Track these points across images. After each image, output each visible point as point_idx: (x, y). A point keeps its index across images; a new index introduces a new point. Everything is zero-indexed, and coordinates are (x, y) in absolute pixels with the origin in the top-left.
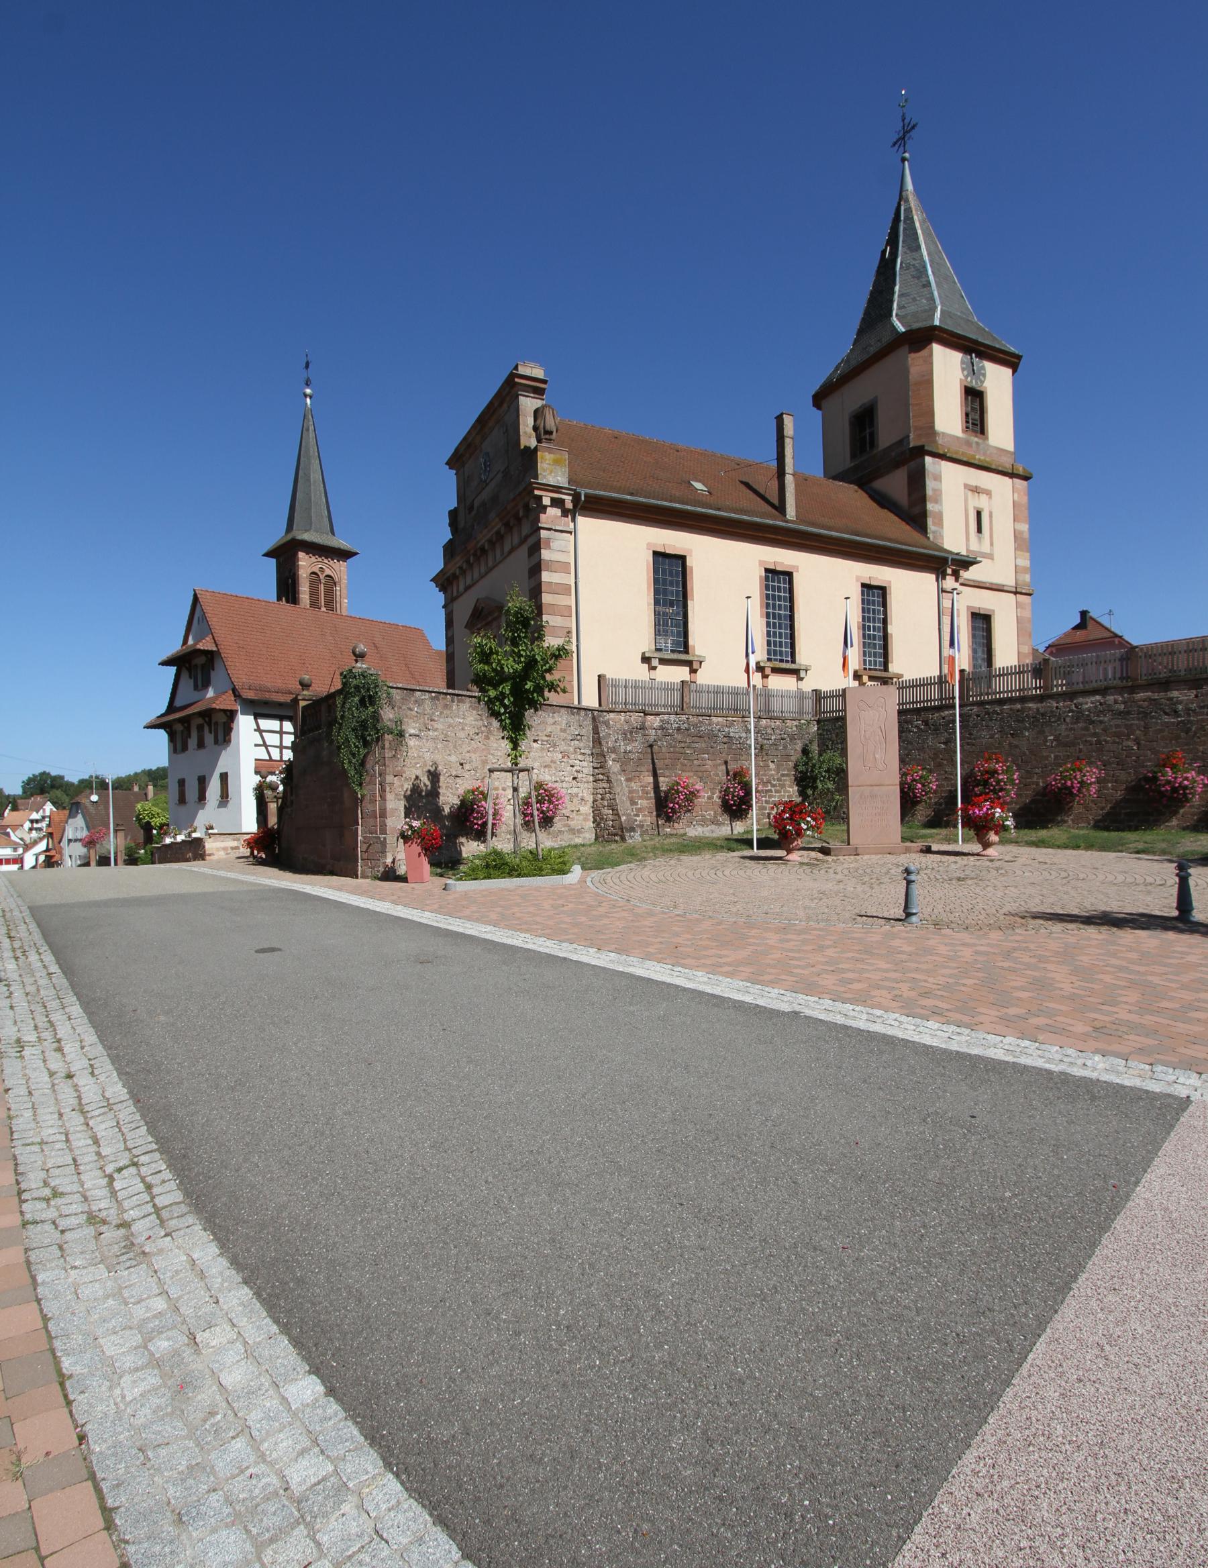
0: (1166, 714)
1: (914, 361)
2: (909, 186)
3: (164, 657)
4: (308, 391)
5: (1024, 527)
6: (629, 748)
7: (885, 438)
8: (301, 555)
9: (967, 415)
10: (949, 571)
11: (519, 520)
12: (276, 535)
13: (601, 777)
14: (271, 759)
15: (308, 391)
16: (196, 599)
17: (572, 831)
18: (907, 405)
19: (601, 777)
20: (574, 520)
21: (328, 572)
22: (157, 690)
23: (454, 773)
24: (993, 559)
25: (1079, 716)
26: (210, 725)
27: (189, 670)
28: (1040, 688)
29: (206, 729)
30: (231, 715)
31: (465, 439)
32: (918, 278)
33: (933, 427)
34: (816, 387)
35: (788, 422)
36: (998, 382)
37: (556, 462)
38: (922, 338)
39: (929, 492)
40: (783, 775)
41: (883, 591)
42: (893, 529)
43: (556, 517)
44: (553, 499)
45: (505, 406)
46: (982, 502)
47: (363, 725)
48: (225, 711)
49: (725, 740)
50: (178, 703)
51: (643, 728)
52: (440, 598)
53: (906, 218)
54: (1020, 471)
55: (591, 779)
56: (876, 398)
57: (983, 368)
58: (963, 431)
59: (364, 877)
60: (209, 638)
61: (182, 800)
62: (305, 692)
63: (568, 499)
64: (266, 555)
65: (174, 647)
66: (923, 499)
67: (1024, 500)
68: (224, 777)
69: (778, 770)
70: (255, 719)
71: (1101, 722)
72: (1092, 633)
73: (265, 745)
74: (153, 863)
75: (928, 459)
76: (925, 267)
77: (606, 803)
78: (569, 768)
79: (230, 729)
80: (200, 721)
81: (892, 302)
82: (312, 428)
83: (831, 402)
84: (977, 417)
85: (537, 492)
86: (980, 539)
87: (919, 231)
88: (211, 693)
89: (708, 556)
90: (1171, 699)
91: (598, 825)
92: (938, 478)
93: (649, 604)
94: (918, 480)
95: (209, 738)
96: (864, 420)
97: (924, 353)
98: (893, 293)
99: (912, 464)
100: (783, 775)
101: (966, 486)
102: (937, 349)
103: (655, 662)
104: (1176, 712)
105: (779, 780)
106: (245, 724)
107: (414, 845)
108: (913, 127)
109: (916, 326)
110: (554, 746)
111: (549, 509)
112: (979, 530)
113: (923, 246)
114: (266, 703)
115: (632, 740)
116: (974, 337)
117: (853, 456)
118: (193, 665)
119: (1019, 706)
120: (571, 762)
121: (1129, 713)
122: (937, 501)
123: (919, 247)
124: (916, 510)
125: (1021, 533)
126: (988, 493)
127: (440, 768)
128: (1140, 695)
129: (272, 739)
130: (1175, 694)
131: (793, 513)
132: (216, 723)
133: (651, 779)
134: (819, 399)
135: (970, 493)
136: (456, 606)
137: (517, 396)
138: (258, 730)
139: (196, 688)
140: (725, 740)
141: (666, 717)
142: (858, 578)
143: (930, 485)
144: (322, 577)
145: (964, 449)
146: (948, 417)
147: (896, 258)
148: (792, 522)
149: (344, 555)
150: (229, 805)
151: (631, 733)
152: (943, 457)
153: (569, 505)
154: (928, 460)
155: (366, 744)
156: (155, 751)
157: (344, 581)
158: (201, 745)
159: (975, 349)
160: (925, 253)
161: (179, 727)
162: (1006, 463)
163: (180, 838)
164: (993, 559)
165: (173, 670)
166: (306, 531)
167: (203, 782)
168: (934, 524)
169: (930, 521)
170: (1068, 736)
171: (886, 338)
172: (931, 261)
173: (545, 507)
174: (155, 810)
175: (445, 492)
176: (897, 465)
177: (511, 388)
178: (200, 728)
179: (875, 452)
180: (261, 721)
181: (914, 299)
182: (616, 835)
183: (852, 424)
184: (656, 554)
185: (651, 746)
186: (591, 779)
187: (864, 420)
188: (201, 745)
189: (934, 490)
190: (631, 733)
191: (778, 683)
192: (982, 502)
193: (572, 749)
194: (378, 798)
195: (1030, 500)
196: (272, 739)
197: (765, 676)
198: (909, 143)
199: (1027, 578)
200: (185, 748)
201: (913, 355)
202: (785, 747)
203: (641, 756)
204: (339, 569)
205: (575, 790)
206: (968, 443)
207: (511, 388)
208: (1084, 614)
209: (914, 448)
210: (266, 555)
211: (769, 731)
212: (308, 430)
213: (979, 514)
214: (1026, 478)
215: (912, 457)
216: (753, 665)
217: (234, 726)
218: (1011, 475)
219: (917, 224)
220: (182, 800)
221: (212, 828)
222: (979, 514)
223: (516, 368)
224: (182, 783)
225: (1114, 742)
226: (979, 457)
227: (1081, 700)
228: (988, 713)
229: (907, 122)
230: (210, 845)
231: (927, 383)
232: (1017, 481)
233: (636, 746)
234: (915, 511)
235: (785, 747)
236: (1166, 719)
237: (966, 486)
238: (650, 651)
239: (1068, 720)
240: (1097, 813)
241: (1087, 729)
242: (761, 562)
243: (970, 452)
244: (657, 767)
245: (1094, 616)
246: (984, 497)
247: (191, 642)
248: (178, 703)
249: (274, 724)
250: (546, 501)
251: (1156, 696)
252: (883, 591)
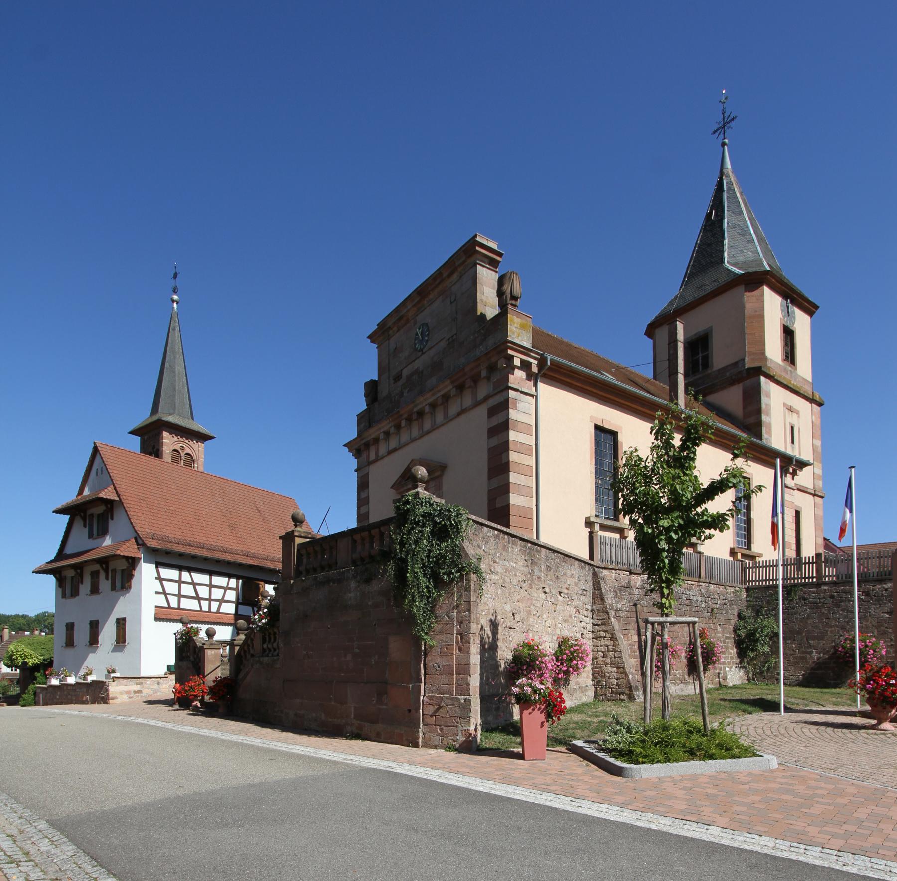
1: (749, 298)
3: (59, 505)
4: (176, 297)
5: (818, 443)
6: (619, 606)
7: (720, 359)
8: (165, 434)
11: (476, 379)
12: (142, 416)
13: (603, 634)
14: (169, 607)
15: (176, 297)
16: (96, 450)
18: (743, 334)
19: (603, 634)
20: (535, 385)
21: (188, 451)
22: (48, 536)
23: (509, 624)
26: (106, 571)
27: (84, 519)
28: (833, 576)
29: (102, 575)
30: (132, 563)
31: (397, 310)
33: (764, 353)
34: (651, 318)
36: (802, 323)
37: (523, 327)
38: (754, 280)
39: (763, 406)
43: (521, 379)
44: (522, 361)
45: (455, 277)
46: (793, 419)
47: (439, 561)
48: (127, 558)
49: (687, 602)
50: (68, 550)
51: (629, 586)
52: (353, 463)
53: (729, 189)
54: (817, 398)
55: (591, 635)
56: (711, 329)
57: (794, 312)
59: (427, 745)
60: (111, 488)
61: (70, 642)
62: (298, 529)
63: (534, 362)
64: (133, 432)
65: (70, 497)
66: (759, 411)
67: (818, 422)
68: (121, 623)
69: (723, 632)
70: (157, 567)
73: (164, 593)
74: (36, 704)
75: (763, 379)
77: (609, 661)
79: (131, 576)
80: (97, 567)
81: (722, 252)
82: (177, 329)
85: (510, 352)
87: (740, 200)
88: (108, 541)
91: (598, 683)
94: (753, 398)
95: (105, 584)
96: (699, 346)
97: (756, 293)
98: (723, 245)
99: (748, 382)
100: (726, 638)
105: (724, 642)
106: (147, 571)
107: (537, 713)
108: (733, 119)
109: (751, 270)
111: (516, 371)
112: (793, 442)
113: (744, 212)
114: (168, 553)
118: (90, 513)
122: (768, 414)
123: (741, 212)
124: (752, 420)
126: (797, 412)
127: (499, 617)
129: (172, 588)
132: (114, 571)
133: (636, 638)
136: (375, 472)
137: (475, 265)
138: (159, 578)
139: (91, 536)
140: (687, 602)
144: (182, 454)
146: (774, 350)
147: (722, 218)
149: (203, 437)
150: (125, 650)
153: (535, 369)
155: (438, 583)
156: (41, 597)
157: (202, 460)
158: (95, 590)
159: (792, 296)
161: (71, 573)
162: (808, 390)
163: (71, 680)
165: (66, 518)
166: (170, 414)
167: (95, 628)
171: (723, 279)
173: (514, 367)
174: (28, 651)
175: (367, 364)
176: (733, 382)
177: (469, 256)
178: (95, 575)
179: (709, 371)
180: (161, 570)
181: (742, 251)
182: (623, 694)
186: (591, 635)
188: (95, 590)
189: (767, 405)
190: (620, 590)
194: (456, 651)
195: (821, 421)
196: (172, 588)
198: (728, 131)
199: (820, 484)
200: (75, 593)
201: (747, 294)
203: (629, 614)
204: (198, 449)
206: (786, 370)
207: (469, 256)
209: (749, 369)
210: (133, 432)
211: (716, 596)
212: (174, 329)
213: (792, 428)
215: (749, 377)
217: (136, 573)
220: (70, 642)
221: (114, 672)
222: (792, 428)
223: (476, 236)
224: (70, 627)
229: (726, 115)
230: (114, 689)
231: (760, 317)
232: (814, 405)
237: (785, 404)
246: (795, 415)
247: (86, 492)
248: (68, 550)
249: (173, 574)
250: (517, 362)
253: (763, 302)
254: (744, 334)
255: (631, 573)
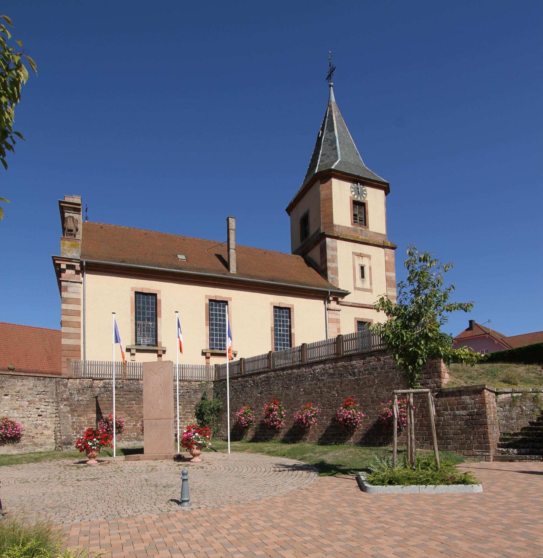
0: (350, 375)
1: (322, 188)
2: (333, 99)
5: (393, 275)
6: (80, 398)
7: (312, 230)
9: (355, 215)
10: (331, 298)
17: (36, 445)
24: (372, 292)
25: (314, 377)
32: (331, 145)
33: (333, 222)
34: (287, 205)
35: (232, 222)
36: (375, 199)
38: (327, 175)
40: (187, 412)
41: (288, 310)
42: (310, 277)
43: (72, 275)
44: (67, 265)
46: (365, 261)
51: (91, 387)
54: (389, 244)
58: (352, 224)
64: (350, 293)
67: (393, 260)
71: (323, 380)
72: (476, 332)
76: (335, 140)
78: (35, 410)
83: (294, 212)
84: (363, 217)
86: (363, 281)
87: (335, 122)
89: (169, 293)
90: (352, 366)
92: (335, 249)
93: (131, 320)
96: (305, 221)
97: (328, 184)
99: (321, 242)
100: (187, 412)
101: (353, 253)
102: (335, 182)
103: (133, 351)
104: (354, 373)
110: (22, 397)
112: (363, 276)
113: (336, 129)
115: (84, 394)
116: (357, 174)
117: (302, 240)
119: (290, 371)
120: (37, 407)
121: (334, 374)
123: (334, 130)
124: (323, 267)
125: (390, 277)
126: (369, 257)
128: (340, 364)
130: (354, 362)
131: (235, 270)
134: (289, 210)
135: (356, 257)
141: (107, 381)
142: (271, 303)
143: (329, 254)
145: (352, 234)
146: (342, 216)
148: (233, 275)
151: (83, 390)
152: (337, 238)
153: (78, 268)
154: (328, 240)
160: (336, 132)
164: (372, 292)
168: (332, 274)
169: (329, 273)
170: (309, 388)
172: (339, 137)
183: (301, 223)
184: (136, 293)
185: (96, 397)
187: (305, 221)
189: (332, 256)
191: (215, 361)
192: (365, 261)
193: (37, 399)
197: (208, 358)
201: (322, 185)
202: (190, 397)
205: (39, 422)
208: (471, 322)
213: (362, 268)
214: (393, 248)
216: (124, 350)
218: (384, 247)
219: (334, 118)
222: (362, 268)
225: (328, 392)
226: (362, 238)
227: (315, 367)
228: (278, 376)
233: (86, 398)
234: (321, 268)
235: (190, 397)
236: (350, 378)
237: (353, 253)
238: (132, 346)
239: (309, 378)
240: (319, 434)
241: (316, 384)
242: (206, 296)
243: (356, 235)
244: (101, 407)
245: (477, 323)
251: (346, 364)
252: (288, 310)
253: (331, 189)
254: (320, 211)
255: (93, 380)
